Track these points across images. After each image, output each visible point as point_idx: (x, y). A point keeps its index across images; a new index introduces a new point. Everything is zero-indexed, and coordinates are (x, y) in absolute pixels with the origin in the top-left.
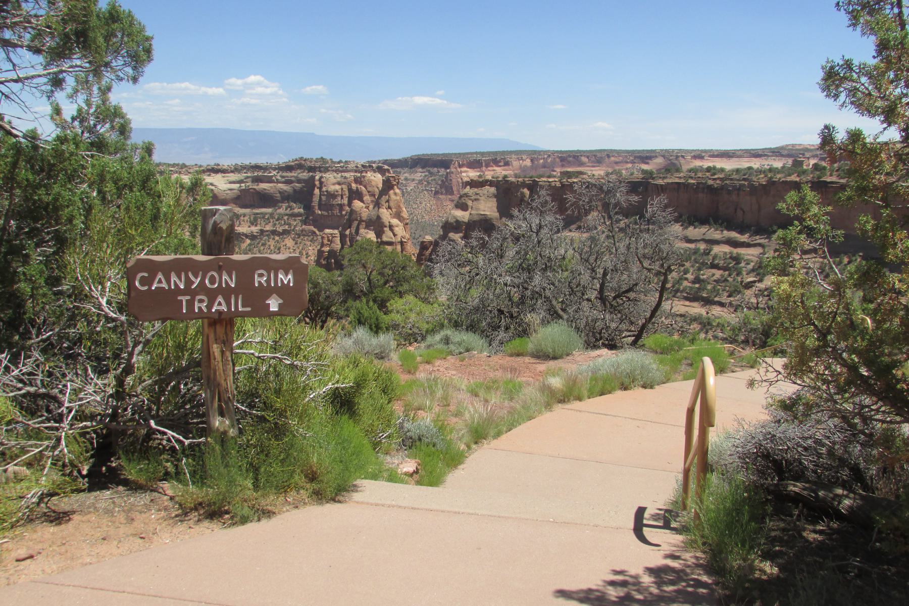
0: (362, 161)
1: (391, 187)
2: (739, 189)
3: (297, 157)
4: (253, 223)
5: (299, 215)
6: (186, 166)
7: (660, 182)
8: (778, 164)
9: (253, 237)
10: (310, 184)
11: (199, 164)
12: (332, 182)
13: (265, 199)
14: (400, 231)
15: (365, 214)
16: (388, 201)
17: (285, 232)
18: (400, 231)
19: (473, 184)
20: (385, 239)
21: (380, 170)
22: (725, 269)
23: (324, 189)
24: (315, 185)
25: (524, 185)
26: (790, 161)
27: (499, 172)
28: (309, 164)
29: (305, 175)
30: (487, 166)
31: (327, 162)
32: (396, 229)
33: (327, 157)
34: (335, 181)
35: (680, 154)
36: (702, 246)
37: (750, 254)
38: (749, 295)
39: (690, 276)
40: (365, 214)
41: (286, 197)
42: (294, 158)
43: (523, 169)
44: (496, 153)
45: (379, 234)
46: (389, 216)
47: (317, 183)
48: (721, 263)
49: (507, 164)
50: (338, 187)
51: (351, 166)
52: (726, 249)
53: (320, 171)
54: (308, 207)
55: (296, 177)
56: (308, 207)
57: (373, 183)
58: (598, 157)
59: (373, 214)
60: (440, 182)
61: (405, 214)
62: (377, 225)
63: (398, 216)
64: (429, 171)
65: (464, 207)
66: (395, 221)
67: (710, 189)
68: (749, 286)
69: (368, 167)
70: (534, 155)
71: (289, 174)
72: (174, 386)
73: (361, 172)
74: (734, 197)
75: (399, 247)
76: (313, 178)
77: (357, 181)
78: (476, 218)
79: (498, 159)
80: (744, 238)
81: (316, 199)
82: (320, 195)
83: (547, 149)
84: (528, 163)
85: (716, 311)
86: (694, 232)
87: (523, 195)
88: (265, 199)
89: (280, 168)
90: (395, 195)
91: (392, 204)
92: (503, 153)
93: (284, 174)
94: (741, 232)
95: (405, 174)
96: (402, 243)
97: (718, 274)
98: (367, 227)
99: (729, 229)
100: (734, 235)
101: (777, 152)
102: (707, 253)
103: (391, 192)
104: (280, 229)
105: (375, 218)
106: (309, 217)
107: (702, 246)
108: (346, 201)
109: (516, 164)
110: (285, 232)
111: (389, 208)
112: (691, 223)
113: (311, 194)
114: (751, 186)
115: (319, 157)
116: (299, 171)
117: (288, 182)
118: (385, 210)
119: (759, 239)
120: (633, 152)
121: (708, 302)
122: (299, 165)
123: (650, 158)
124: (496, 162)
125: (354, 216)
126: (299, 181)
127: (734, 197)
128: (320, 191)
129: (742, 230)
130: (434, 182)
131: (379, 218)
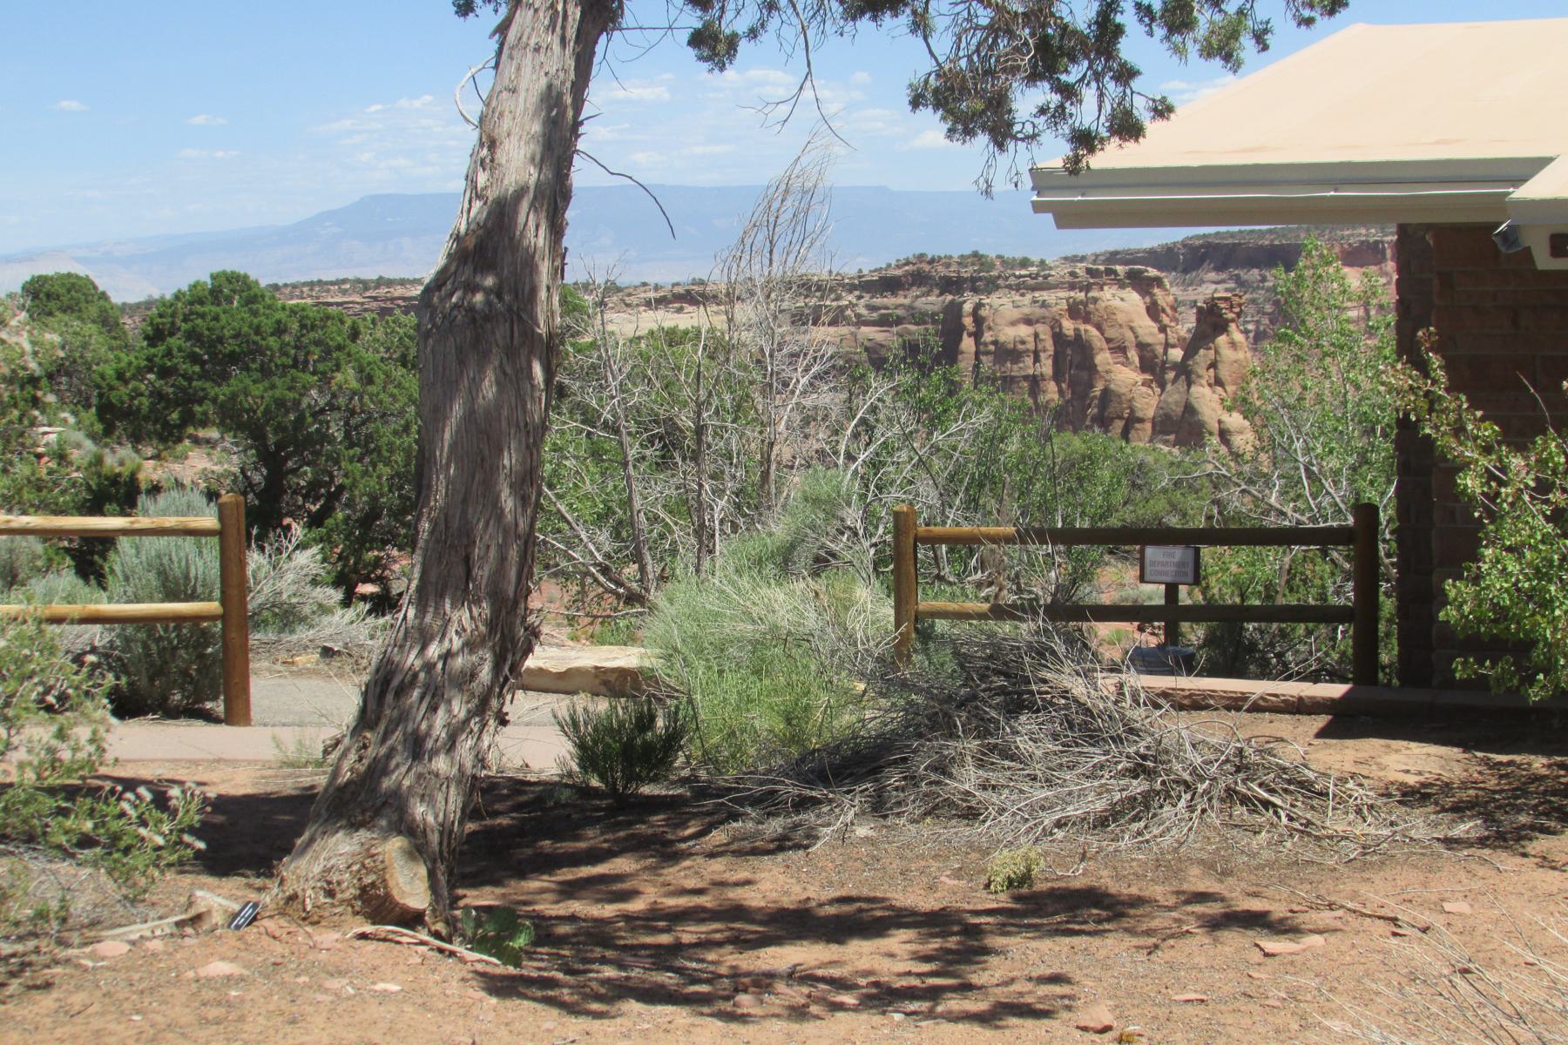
1: (1221, 327)
3: (909, 252)
6: (619, 290)
11: (652, 281)
16: (1213, 365)
23: (987, 337)
24: (962, 328)
28: (942, 271)
29: (933, 302)
31: (992, 266)
32: (1238, 441)
33: (930, 253)
34: (1016, 314)
42: (902, 257)
46: (1218, 407)
47: (968, 321)
50: (1024, 331)
53: (975, 290)
55: (910, 307)
57: (1120, 318)
60: (1268, 308)
64: (1238, 280)
66: (1235, 420)
71: (890, 300)
72: (502, 830)
73: (1087, 288)
76: (954, 311)
77: (1074, 311)
82: (977, 354)
89: (866, 286)
91: (1224, 372)
93: (878, 301)
103: (1222, 340)
105: (1180, 410)
108: (1047, 367)
111: (1218, 382)
115: (967, 252)
116: (915, 291)
118: (1207, 390)
122: (917, 276)
125: (1112, 409)
126: (920, 318)
128: (977, 343)
130: (1251, 310)
131: (1189, 409)
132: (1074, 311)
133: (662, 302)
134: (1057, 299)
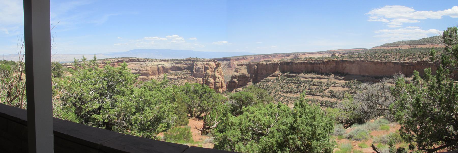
0: (208, 59)
1: (219, 66)
2: (320, 63)
4: (175, 75)
5: (189, 73)
7: (296, 62)
8: (327, 56)
9: (175, 79)
10: (193, 65)
12: (199, 64)
13: (179, 69)
14: (221, 79)
15: (210, 74)
17: (185, 78)
18: (221, 79)
19: (239, 65)
20: (216, 81)
21: (214, 61)
22: (317, 85)
25: (255, 65)
26: (331, 55)
27: (245, 61)
29: (191, 62)
30: (241, 59)
35: (298, 54)
36: (310, 79)
37: (324, 81)
38: (326, 93)
39: (307, 88)
40: (210, 74)
41: (185, 68)
43: (252, 60)
44: (243, 56)
45: (215, 79)
48: (316, 84)
49: (247, 59)
50: (201, 66)
51: (205, 60)
52: (318, 80)
54: (192, 71)
56: (192, 71)
58: (274, 56)
59: (213, 74)
61: (222, 74)
62: (214, 77)
63: (221, 74)
65: (237, 72)
66: (219, 76)
67: (311, 63)
68: (325, 90)
69: (210, 60)
70: (255, 56)
74: (318, 65)
75: (221, 83)
76: (194, 63)
77: (207, 64)
78: (241, 74)
79: (244, 58)
80: (322, 76)
81: (194, 69)
83: (258, 54)
84: (253, 58)
85: (316, 97)
86: (307, 75)
87: (255, 67)
88: (179, 69)
89: (184, 60)
90: (220, 69)
92: (245, 56)
94: (321, 75)
95: (221, 62)
96: (221, 82)
97: (316, 87)
98: (211, 77)
99: (318, 74)
100: (319, 76)
101: (326, 52)
102: (312, 81)
104: (183, 77)
106: (192, 74)
107: (310, 79)
108: (203, 70)
109: (249, 59)
110: (185, 78)
112: (306, 73)
113: (193, 67)
114: (323, 62)
117: (186, 64)
119: (327, 77)
120: (284, 54)
121: (313, 95)
123: (289, 55)
124: (243, 58)
126: (189, 64)
127: (318, 65)
129: (321, 74)
131: (215, 75)
132: (207, 64)
133: (160, 61)
134: (205, 63)
